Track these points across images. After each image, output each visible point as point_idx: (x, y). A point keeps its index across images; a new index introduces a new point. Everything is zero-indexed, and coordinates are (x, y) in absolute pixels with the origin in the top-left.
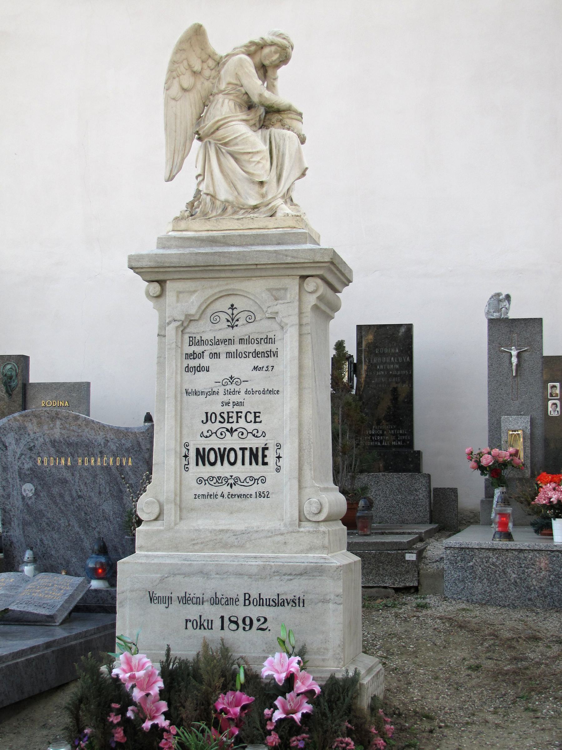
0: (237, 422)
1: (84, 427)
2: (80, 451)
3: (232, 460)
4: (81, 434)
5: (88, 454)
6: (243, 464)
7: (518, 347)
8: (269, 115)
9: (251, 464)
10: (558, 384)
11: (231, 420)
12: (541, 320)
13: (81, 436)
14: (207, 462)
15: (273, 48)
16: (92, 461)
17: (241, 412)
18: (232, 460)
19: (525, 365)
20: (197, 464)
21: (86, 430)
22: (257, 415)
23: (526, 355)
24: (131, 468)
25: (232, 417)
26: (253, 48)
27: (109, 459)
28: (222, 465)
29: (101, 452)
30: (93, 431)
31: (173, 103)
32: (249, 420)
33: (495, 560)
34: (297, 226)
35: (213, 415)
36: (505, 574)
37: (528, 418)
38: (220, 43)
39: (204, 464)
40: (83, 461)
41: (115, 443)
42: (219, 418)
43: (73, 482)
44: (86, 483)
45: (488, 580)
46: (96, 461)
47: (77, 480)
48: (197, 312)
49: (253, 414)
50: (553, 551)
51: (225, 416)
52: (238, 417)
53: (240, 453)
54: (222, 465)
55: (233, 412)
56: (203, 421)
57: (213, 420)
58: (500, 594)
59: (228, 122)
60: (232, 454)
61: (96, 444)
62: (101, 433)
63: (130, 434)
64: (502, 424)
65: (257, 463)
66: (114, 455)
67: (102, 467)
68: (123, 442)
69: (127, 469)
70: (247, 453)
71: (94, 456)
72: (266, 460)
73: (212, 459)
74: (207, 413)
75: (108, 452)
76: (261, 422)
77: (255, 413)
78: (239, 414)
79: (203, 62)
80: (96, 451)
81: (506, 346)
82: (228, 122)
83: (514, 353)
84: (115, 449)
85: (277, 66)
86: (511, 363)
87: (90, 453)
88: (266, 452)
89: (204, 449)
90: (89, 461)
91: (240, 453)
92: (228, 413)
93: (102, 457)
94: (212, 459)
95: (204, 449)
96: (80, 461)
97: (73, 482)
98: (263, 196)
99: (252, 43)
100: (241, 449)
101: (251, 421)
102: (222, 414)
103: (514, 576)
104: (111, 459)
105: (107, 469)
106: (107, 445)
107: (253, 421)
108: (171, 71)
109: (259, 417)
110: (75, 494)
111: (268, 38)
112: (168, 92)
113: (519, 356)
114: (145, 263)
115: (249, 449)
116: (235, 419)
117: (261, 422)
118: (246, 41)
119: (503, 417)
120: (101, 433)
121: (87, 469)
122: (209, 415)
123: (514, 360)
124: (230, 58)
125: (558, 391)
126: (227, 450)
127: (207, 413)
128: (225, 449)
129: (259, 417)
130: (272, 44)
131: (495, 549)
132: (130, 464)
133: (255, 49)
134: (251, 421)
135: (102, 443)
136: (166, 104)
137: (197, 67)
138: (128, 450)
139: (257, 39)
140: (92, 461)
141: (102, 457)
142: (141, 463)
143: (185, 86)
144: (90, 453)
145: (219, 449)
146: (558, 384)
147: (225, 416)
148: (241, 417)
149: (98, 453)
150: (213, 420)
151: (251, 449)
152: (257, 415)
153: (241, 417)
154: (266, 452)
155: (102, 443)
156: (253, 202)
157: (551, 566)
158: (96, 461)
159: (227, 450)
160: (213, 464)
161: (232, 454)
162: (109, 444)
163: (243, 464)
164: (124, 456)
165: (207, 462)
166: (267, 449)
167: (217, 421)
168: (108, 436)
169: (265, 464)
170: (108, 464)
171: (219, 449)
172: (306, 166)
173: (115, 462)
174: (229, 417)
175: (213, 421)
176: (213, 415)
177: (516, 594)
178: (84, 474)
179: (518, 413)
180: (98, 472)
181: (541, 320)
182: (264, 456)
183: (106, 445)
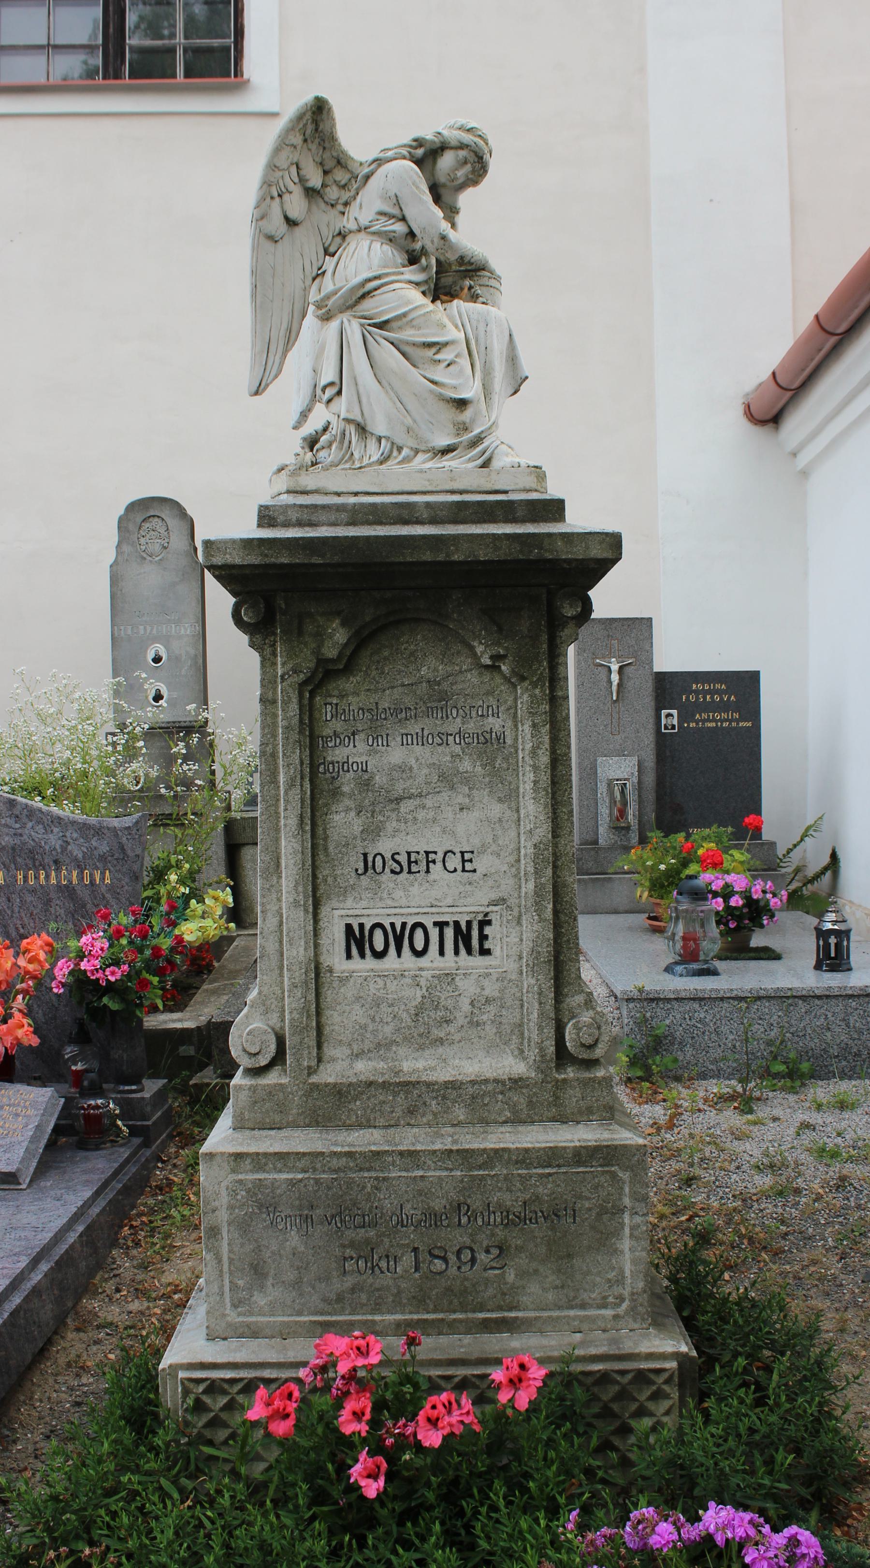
0: (428, 871)
1: (25, 820)
2: (19, 860)
3: (419, 946)
4: (19, 831)
5: (34, 865)
6: (442, 953)
7: (619, 658)
8: (455, 277)
9: (457, 952)
10: (675, 712)
11: (414, 868)
12: (650, 620)
13: (21, 835)
14: (368, 952)
15: (462, 153)
16: (42, 877)
17: (435, 853)
18: (419, 946)
19: (629, 685)
20: (349, 956)
21: (30, 824)
22: (467, 856)
23: (629, 671)
24: (111, 888)
25: (416, 862)
26: (420, 152)
27: (70, 873)
28: (399, 955)
29: (56, 862)
30: (41, 826)
31: (268, 245)
32: (450, 866)
33: (702, 1016)
34: (539, 488)
35: (379, 858)
36: (718, 1034)
37: (634, 760)
38: (356, 139)
39: (362, 956)
40: (26, 878)
41: (80, 846)
42: (391, 863)
43: (9, 912)
44: (32, 914)
45: (693, 1046)
46: (47, 877)
47: (16, 909)
48: (340, 654)
49: (459, 855)
50: (788, 998)
51: (403, 859)
52: (428, 862)
53: (434, 933)
54: (399, 955)
55: (418, 853)
56: (357, 870)
57: (379, 868)
58: (711, 1067)
59: (382, 285)
60: (419, 934)
61: (47, 848)
62: (56, 830)
63: (106, 831)
64: (599, 770)
65: (469, 952)
66: (79, 866)
67: (59, 887)
68: (94, 844)
69: (103, 889)
70: (449, 933)
71: (44, 869)
72: (487, 946)
73: (379, 946)
74: (365, 855)
75: (67, 861)
76: (475, 871)
77: (462, 853)
78: (432, 856)
79: (326, 173)
80: (47, 860)
81: (603, 657)
82: (382, 285)
83: (615, 667)
84: (80, 856)
85: (462, 187)
86: (610, 682)
87: (37, 863)
88: (487, 930)
89: (361, 926)
90: (37, 878)
91: (434, 933)
92: (409, 854)
93: (58, 870)
94: (379, 946)
95: (361, 926)
96: (20, 877)
97: (9, 912)
98: (464, 428)
99: (419, 142)
100: (436, 924)
101: (455, 870)
102: (396, 857)
103: (731, 1037)
104: (75, 874)
105: (68, 891)
106: (66, 849)
107: (460, 868)
108: (267, 183)
109: (471, 861)
110: (14, 934)
111: (453, 136)
112: (260, 223)
113: (621, 670)
114: (236, 558)
115: (452, 924)
116: (423, 866)
117: (475, 871)
118: (407, 139)
119: (600, 760)
120: (56, 830)
121: (33, 891)
122: (370, 859)
123: (615, 678)
124: (380, 166)
125: (675, 722)
126: (408, 927)
127: (365, 855)
128: (404, 925)
129: (471, 861)
130: (462, 146)
131: (704, 999)
132: (107, 881)
133: (426, 155)
134: (455, 870)
135: (58, 847)
136: (256, 248)
137: (315, 180)
138: (103, 858)
139: (428, 134)
140: (42, 877)
141: (58, 870)
142: (127, 880)
143: (293, 215)
144: (37, 863)
145: (392, 925)
146: (675, 712)
147: (403, 859)
148: (434, 862)
149: (51, 863)
150: (379, 868)
151: (457, 924)
152: (467, 856)
153: (434, 862)
154: (487, 930)
155: (58, 847)
156: (444, 441)
157: (786, 1019)
158: (47, 877)
159: (408, 927)
160: (379, 955)
161: (419, 934)
162: (69, 848)
163: (442, 953)
164: (97, 868)
165: (368, 952)
166: (489, 923)
167: (387, 870)
168: (68, 834)
169: (485, 952)
170: (70, 882)
171: (392, 925)
172: (527, 374)
173: (81, 878)
174: (410, 863)
175: (379, 870)
176: (379, 858)
177: (735, 1065)
178: (29, 898)
179: (621, 754)
180: (53, 895)
181: (650, 620)
182: (483, 938)
183: (64, 849)
